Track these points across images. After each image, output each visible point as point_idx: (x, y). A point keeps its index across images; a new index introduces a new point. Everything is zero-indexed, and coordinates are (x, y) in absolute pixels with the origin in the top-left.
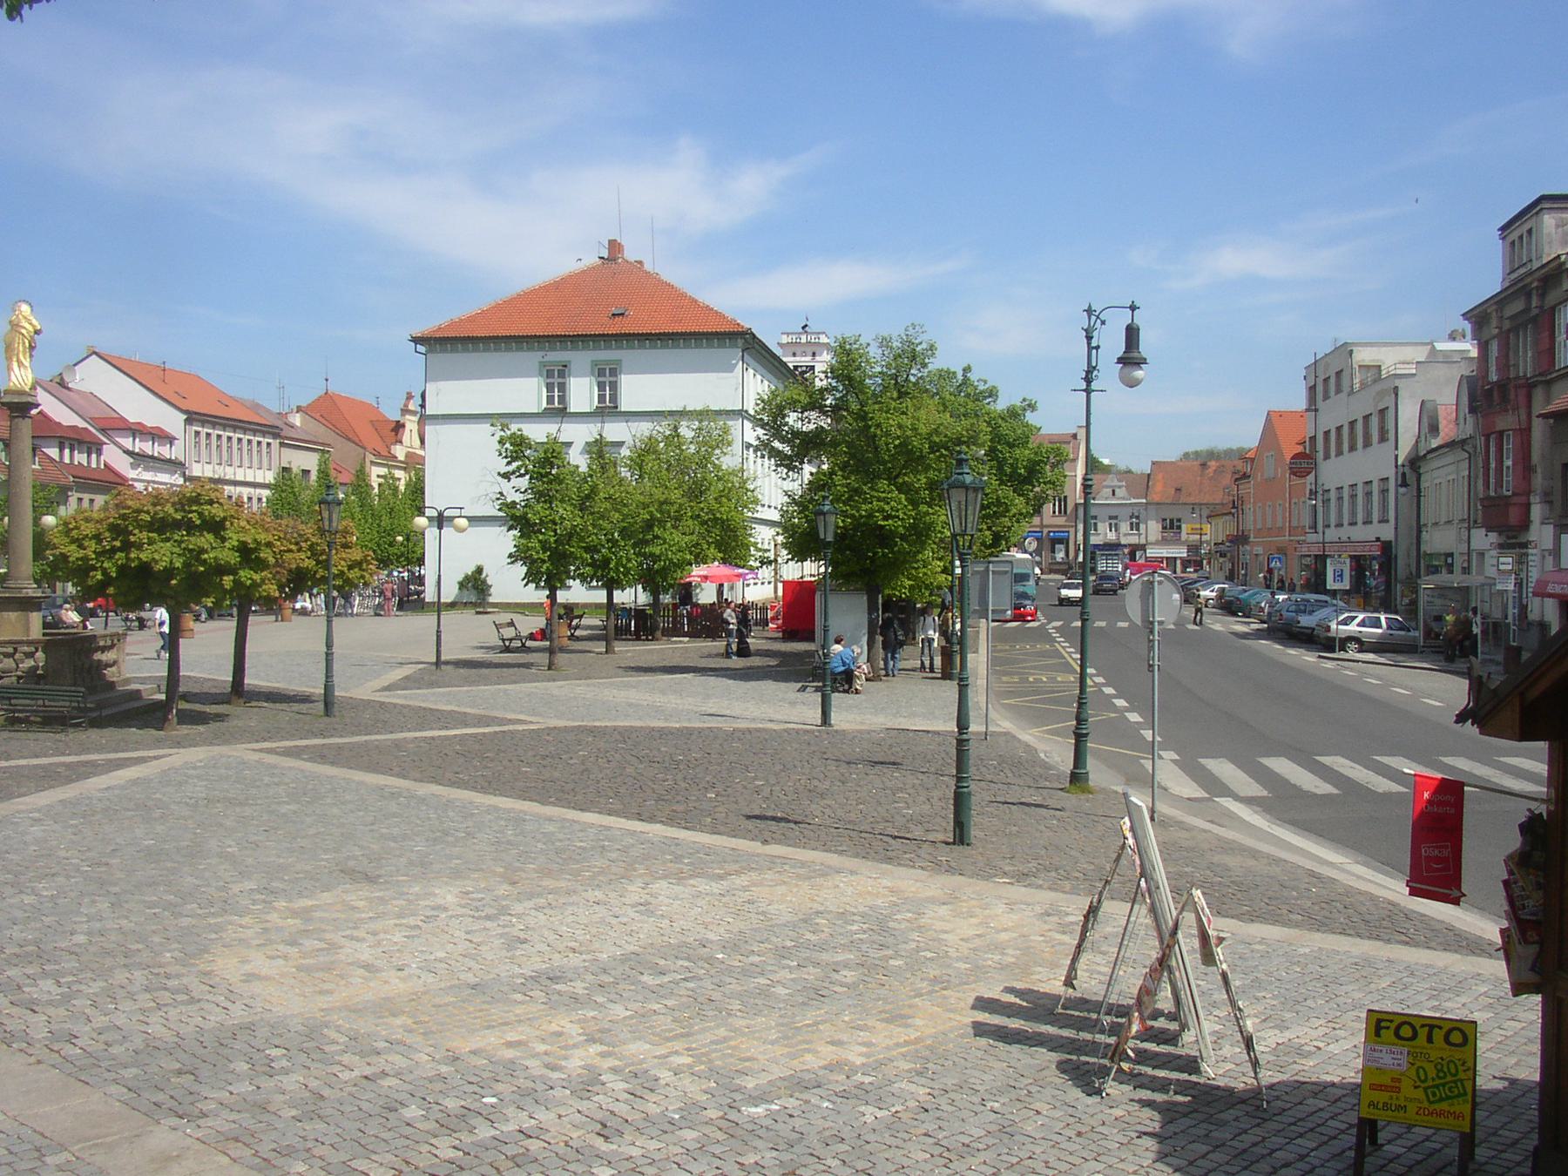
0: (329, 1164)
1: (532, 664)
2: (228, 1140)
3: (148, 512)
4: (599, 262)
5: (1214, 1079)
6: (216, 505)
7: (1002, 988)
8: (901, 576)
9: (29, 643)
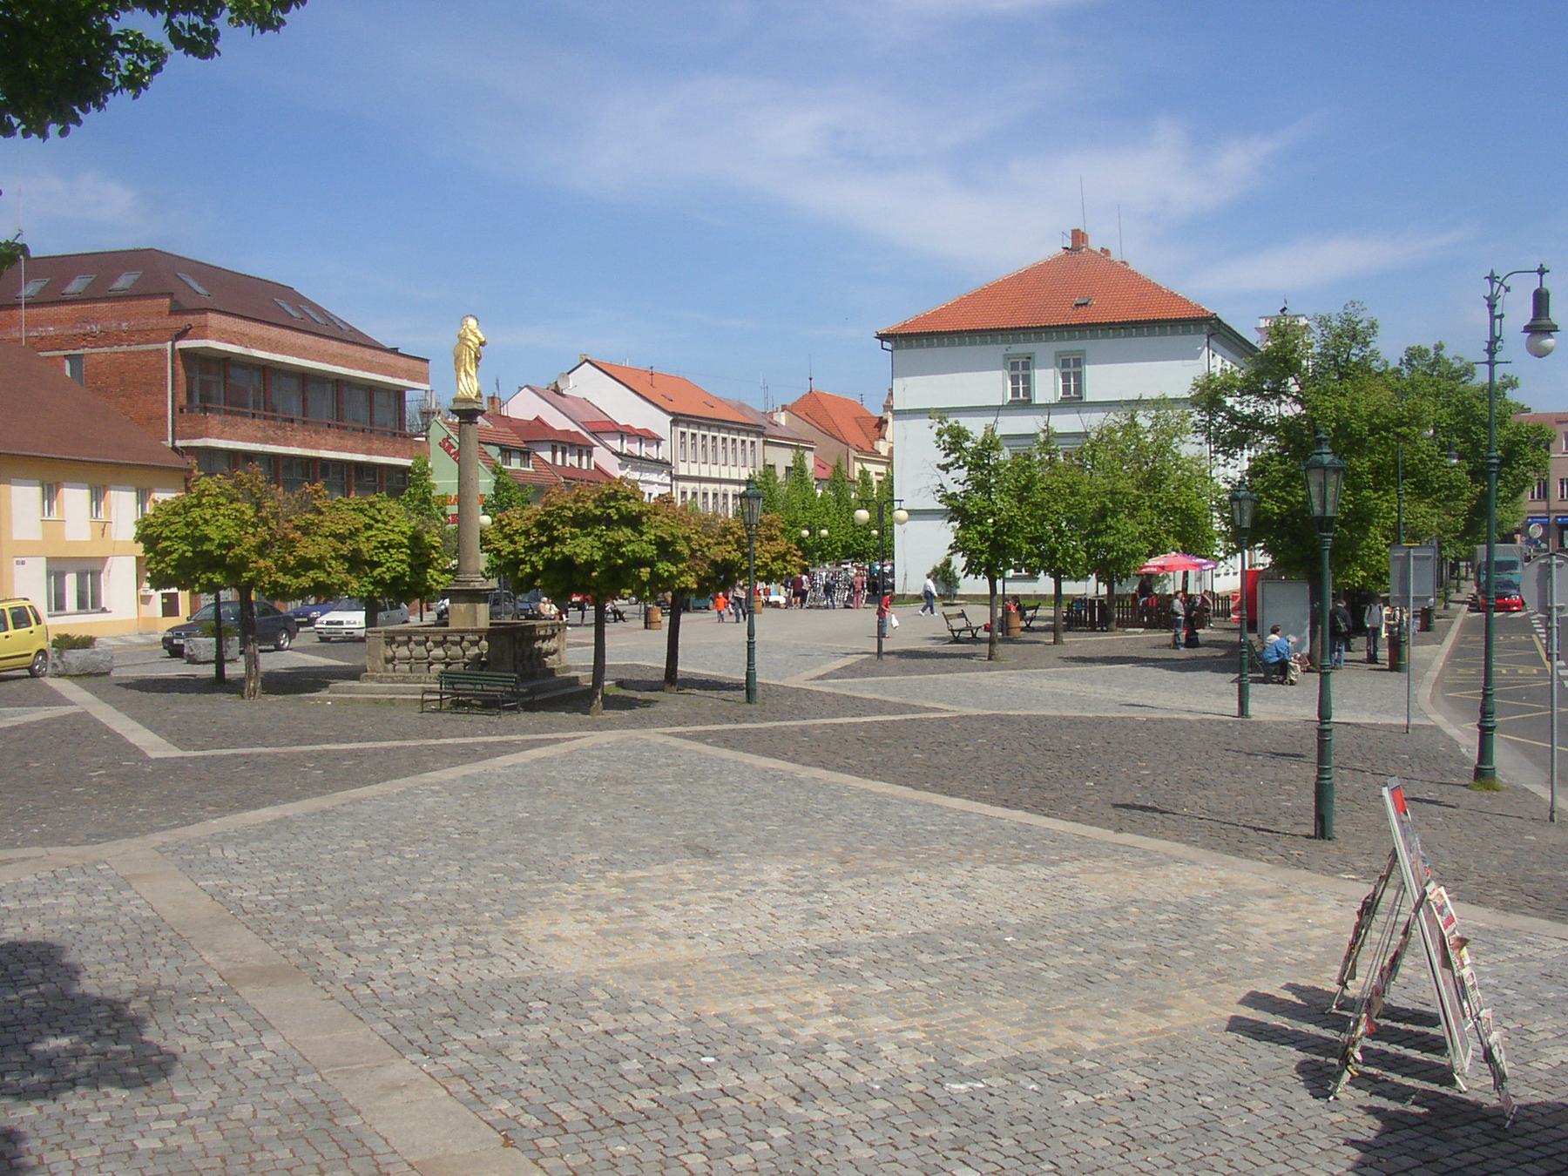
0: (530, 1104)
1: (975, 655)
2: (454, 1076)
3: (570, 509)
4: (1063, 252)
5: (1465, 1092)
6: (632, 501)
7: (1284, 984)
8: (1353, 564)
9: (474, 632)
